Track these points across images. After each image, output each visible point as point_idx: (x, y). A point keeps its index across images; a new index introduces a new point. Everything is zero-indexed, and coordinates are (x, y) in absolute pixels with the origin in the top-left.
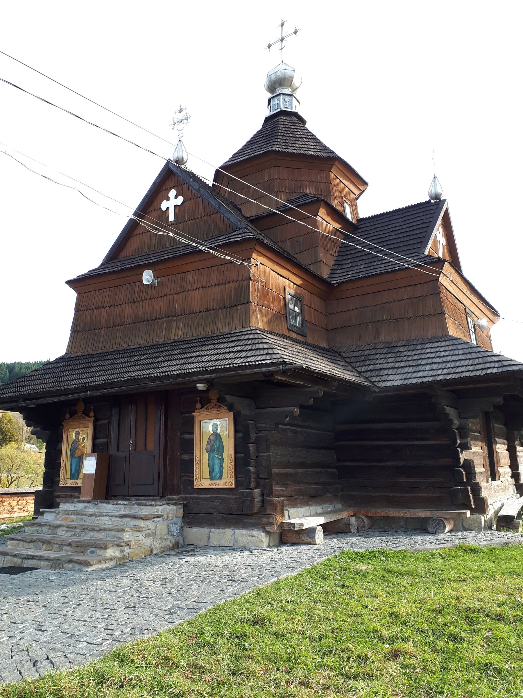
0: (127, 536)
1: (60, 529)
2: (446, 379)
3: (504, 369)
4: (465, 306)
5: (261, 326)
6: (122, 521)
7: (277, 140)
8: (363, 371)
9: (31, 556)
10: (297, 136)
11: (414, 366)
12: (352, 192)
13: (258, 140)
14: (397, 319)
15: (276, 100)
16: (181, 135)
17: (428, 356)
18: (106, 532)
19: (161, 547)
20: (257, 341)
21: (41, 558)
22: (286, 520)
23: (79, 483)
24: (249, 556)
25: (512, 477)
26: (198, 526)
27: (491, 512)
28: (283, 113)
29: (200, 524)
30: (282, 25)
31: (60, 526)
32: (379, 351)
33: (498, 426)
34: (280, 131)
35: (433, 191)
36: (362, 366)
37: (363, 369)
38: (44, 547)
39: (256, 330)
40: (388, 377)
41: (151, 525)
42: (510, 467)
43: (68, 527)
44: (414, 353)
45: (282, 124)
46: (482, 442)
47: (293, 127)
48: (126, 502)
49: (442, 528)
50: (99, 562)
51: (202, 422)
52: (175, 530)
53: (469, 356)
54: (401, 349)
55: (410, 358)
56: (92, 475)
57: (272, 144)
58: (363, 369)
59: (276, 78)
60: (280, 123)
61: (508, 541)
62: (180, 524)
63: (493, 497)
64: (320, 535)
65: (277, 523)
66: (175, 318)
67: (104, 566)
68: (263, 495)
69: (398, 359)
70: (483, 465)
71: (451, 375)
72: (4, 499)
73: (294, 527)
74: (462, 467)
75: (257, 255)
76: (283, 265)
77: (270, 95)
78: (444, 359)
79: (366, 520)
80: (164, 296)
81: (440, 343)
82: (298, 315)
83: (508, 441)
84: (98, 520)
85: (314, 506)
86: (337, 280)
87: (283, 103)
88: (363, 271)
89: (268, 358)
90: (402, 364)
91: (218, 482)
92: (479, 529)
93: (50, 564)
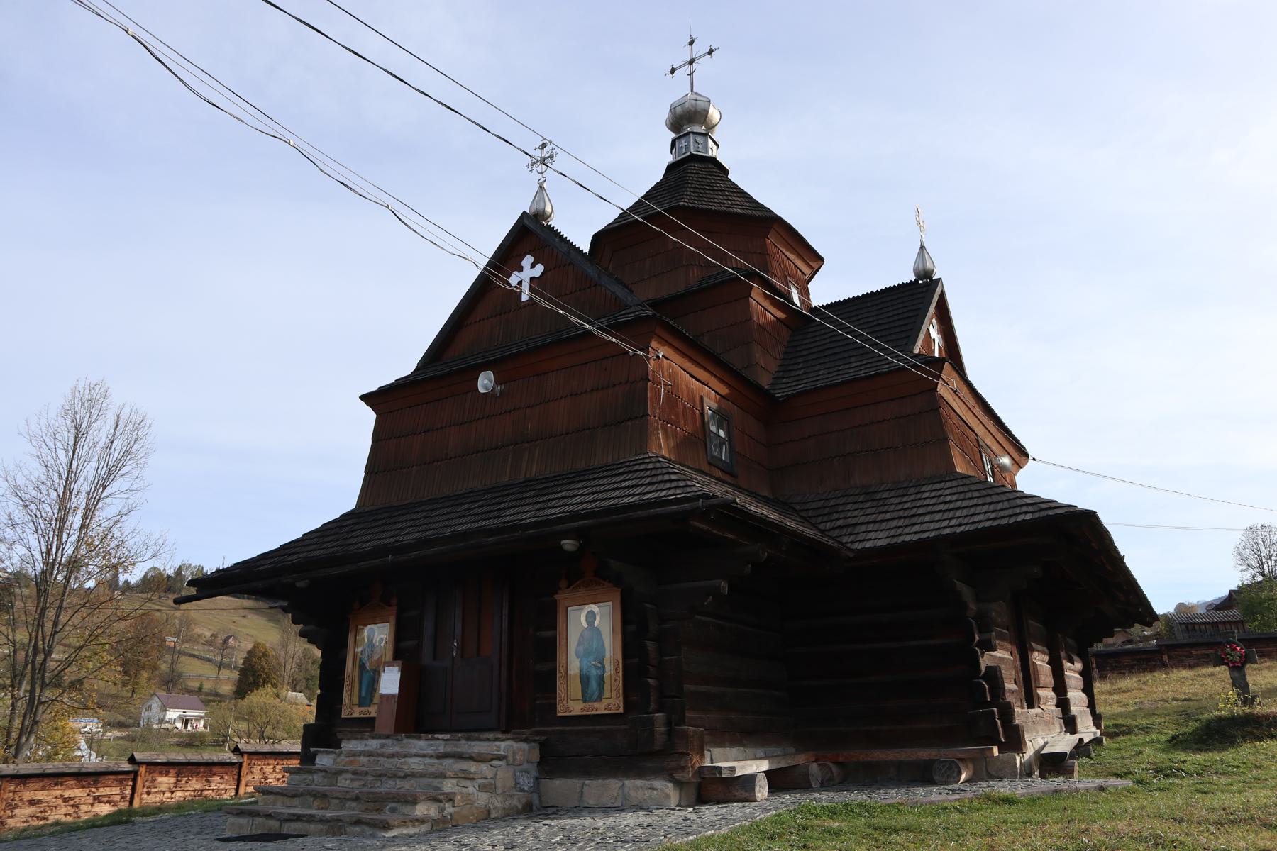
0: (448, 786)
1: (342, 777)
2: (955, 533)
3: (1043, 514)
4: (976, 435)
5: (664, 452)
6: (441, 764)
7: (685, 193)
8: (827, 528)
9: (294, 815)
10: (716, 188)
11: (905, 517)
12: (800, 270)
13: (658, 194)
14: (877, 450)
15: (683, 142)
16: (543, 180)
17: (927, 502)
18: (415, 779)
19: (504, 808)
20: (659, 471)
21: (310, 819)
22: (708, 764)
23: (373, 711)
24: (648, 816)
25: (1057, 706)
26: (563, 777)
27: (1030, 752)
28: (693, 158)
29: (566, 773)
30: (691, 43)
31: (341, 772)
32: (850, 499)
33: (1033, 625)
34: (690, 181)
35: (921, 267)
36: (826, 522)
37: (828, 525)
38: (316, 803)
39: (657, 457)
40: (866, 535)
41: (487, 772)
42: (1054, 690)
43: (354, 773)
44: (905, 499)
45: (693, 173)
46: (1011, 645)
47: (709, 177)
48: (447, 736)
49: (955, 774)
50: (404, 824)
51: (569, 609)
52: (527, 782)
53: (988, 500)
54: (885, 495)
55: (900, 507)
56: (393, 696)
57: (678, 198)
58: (828, 525)
59: (683, 111)
60: (689, 171)
61: (1059, 787)
62: (534, 773)
63: (1032, 731)
64: (762, 791)
65: (692, 767)
66: (526, 445)
67: (412, 831)
68: (669, 723)
69: (881, 509)
70: (1015, 680)
71: (963, 527)
72: (253, 761)
73: (720, 773)
74: (984, 678)
75: (659, 343)
76: (699, 361)
77: (673, 135)
78: (952, 506)
79: (835, 769)
80: (510, 412)
81: (943, 484)
82: (725, 444)
83: (1049, 649)
84: (402, 764)
85: (750, 747)
86: (783, 392)
87: (694, 146)
88: (823, 379)
89: (678, 492)
90: (888, 516)
91: (596, 705)
92: (1013, 776)
93: (325, 827)
